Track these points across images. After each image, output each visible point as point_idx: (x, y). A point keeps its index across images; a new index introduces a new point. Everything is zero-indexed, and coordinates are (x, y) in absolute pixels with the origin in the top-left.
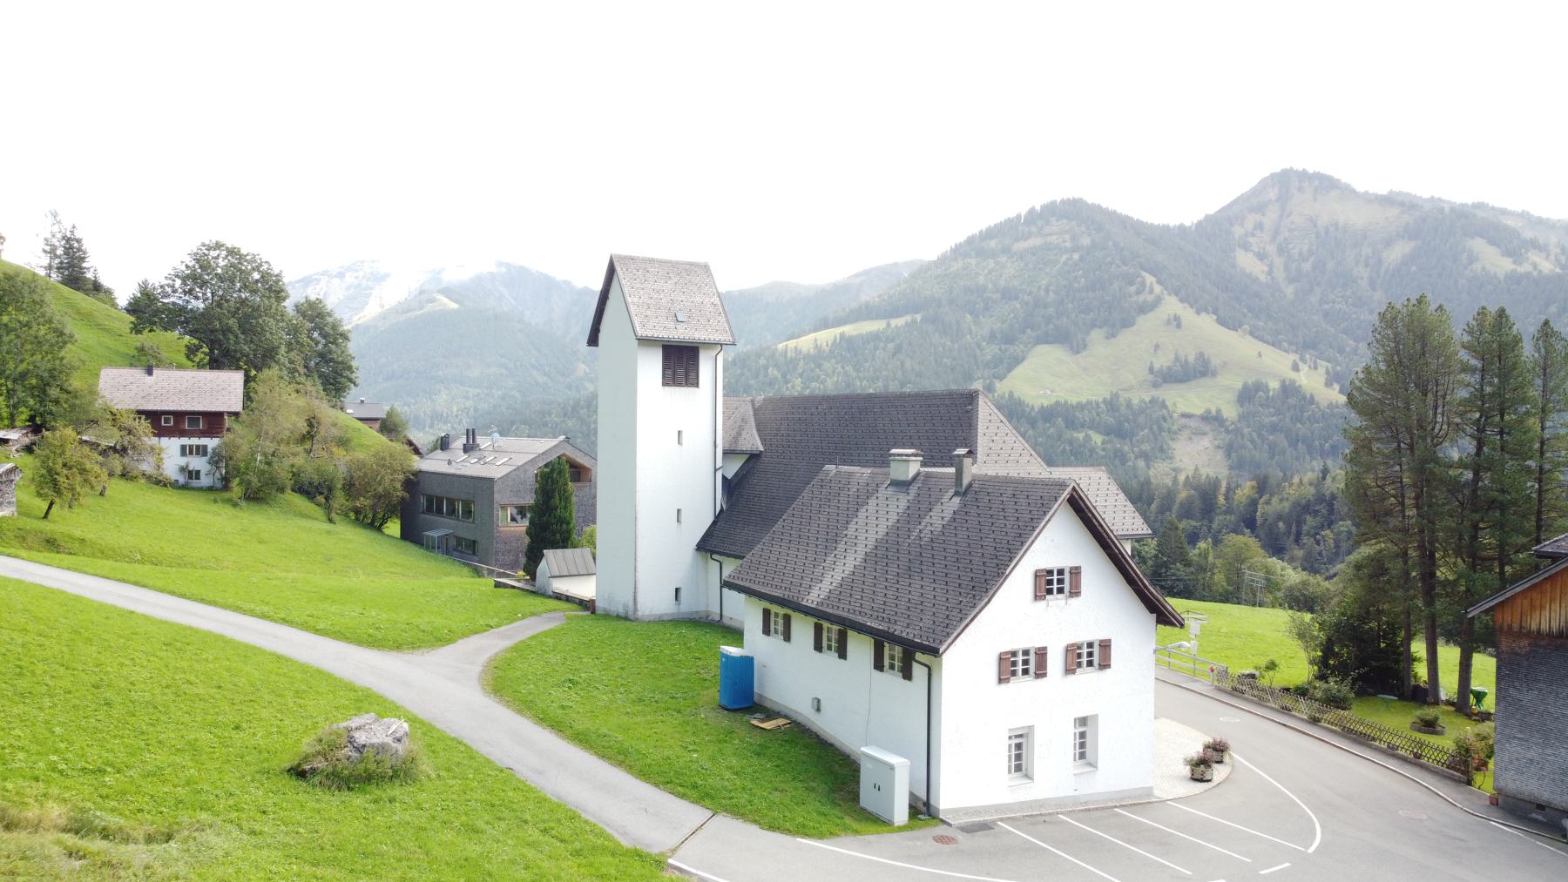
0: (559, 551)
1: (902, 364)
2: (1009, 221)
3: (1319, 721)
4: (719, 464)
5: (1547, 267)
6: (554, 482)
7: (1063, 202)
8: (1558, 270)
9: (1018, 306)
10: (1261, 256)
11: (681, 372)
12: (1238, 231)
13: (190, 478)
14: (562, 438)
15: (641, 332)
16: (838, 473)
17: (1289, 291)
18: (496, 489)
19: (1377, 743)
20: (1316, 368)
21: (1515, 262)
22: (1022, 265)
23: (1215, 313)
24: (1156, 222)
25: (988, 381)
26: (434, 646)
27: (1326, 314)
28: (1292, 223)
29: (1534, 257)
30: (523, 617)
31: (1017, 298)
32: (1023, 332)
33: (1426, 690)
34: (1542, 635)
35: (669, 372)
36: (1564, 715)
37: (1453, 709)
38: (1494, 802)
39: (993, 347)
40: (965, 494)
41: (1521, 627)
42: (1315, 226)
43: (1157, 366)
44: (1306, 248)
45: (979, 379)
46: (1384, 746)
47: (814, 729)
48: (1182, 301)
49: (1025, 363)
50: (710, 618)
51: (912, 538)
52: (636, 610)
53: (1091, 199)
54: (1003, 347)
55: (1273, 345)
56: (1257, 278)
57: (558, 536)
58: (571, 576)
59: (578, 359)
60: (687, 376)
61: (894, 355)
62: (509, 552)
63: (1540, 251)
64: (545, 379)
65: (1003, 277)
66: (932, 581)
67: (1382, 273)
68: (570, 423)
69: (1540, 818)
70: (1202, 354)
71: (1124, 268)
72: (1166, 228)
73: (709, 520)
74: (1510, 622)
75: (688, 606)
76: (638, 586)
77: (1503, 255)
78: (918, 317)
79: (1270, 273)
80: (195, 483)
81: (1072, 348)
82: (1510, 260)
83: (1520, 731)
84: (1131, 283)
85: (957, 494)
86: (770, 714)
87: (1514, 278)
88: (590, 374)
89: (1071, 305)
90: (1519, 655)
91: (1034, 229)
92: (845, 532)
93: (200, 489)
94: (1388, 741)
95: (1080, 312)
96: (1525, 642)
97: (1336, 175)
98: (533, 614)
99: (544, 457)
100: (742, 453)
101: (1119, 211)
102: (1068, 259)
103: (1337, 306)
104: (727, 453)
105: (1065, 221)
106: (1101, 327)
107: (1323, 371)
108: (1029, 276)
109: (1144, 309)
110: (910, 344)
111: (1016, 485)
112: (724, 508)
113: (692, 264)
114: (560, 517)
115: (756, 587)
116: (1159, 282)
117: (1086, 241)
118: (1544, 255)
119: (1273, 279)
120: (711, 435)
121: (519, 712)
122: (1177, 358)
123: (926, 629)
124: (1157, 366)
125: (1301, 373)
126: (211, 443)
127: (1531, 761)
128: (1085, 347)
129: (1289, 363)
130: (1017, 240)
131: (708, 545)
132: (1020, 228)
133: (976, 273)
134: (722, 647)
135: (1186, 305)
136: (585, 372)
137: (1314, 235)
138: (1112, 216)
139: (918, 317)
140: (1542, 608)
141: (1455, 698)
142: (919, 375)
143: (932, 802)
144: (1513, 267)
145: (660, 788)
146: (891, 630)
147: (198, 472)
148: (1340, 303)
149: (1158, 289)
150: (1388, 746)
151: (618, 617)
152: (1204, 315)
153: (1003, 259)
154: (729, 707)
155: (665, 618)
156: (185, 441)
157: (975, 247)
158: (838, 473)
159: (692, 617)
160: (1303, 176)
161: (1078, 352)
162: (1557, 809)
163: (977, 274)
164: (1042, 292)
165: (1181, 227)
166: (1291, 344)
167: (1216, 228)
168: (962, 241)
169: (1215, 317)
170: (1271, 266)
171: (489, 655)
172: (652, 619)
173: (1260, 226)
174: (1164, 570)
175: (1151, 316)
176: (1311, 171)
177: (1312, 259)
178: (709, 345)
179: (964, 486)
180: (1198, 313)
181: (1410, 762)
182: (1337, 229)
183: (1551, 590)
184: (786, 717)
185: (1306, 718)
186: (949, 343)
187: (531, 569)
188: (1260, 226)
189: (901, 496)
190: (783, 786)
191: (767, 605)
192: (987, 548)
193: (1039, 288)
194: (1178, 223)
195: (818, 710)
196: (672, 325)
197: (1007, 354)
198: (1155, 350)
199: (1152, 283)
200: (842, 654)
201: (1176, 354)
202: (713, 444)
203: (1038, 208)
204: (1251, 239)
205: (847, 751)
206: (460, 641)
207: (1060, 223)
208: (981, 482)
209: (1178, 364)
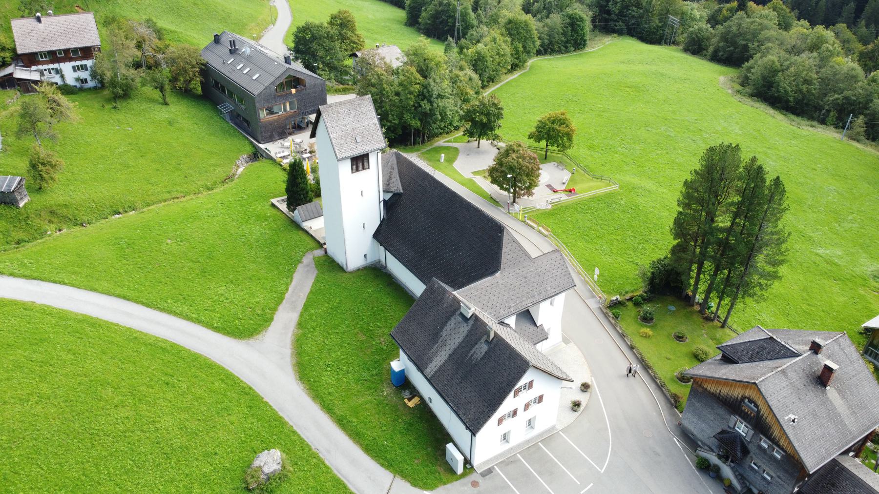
13: (83, 83)
33: (690, 297)
46: (653, 375)
62: (268, 131)
80: (86, 86)
93: (90, 89)
100: (392, 192)
120: (377, 186)
121: (313, 399)
126: (89, 63)
143: (472, 462)
147: (86, 80)
156: (74, 63)
174: (625, 11)
196: (354, 146)
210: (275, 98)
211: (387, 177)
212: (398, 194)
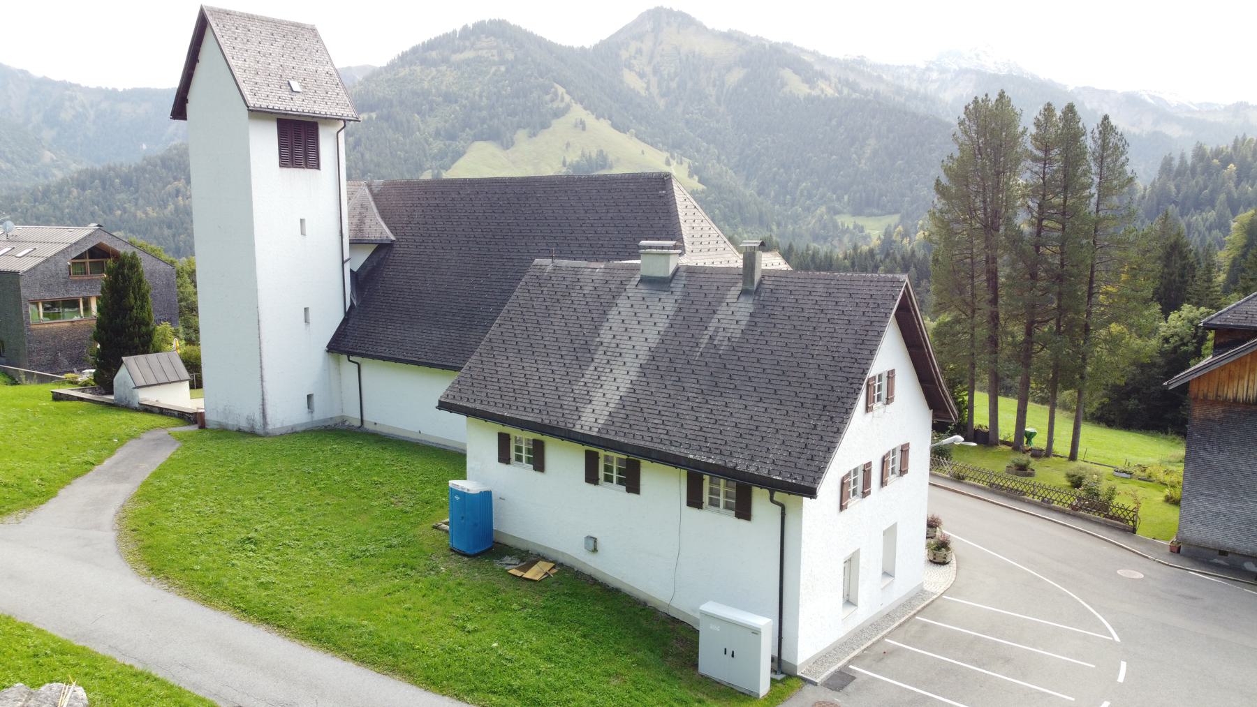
0: (141, 358)
1: (362, 155)
2: (446, 36)
3: (963, 478)
4: (346, 256)
5: (830, 92)
6: (127, 279)
7: (491, 22)
8: (836, 95)
9: (458, 108)
10: (641, 75)
11: (299, 150)
12: (624, 55)
14: (93, 226)
15: (252, 102)
16: (556, 268)
17: (662, 103)
18: (22, 284)
19: (1030, 497)
20: (681, 163)
21: (810, 88)
22: (459, 74)
23: (610, 119)
24: (563, 44)
25: (436, 171)
26: (29, 505)
27: (687, 122)
28: (663, 50)
29: (822, 84)
30: (122, 442)
31: (456, 102)
32: (463, 131)
34: (1239, 402)
35: (286, 151)
36: (1254, 473)
37: (1010, 448)
38: (1176, 550)
39: (438, 142)
40: (757, 292)
41: (1217, 396)
42: (679, 54)
43: (568, 160)
44: (673, 70)
45: (428, 169)
46: (984, 485)
47: (588, 571)
48: (585, 108)
49: (466, 157)
50: (347, 423)
51: (703, 346)
52: (265, 424)
53: (513, 21)
54: (447, 143)
55: (652, 145)
56: (638, 92)
57: (136, 340)
58: (159, 384)
59: (43, 147)
60: (306, 156)
61: (354, 148)
62: (45, 351)
63: (826, 80)
64: (9, 165)
65: (445, 83)
66: (758, 399)
67: (725, 91)
68: (41, 208)
69: (1222, 562)
70: (601, 152)
71: (541, 80)
72: (571, 49)
73: (339, 317)
74: (1205, 391)
75: (323, 412)
76: (265, 397)
77: (803, 82)
78: (374, 115)
79: (647, 89)
81: (502, 144)
82: (807, 86)
83: (1208, 489)
84: (547, 93)
85: (745, 292)
86: (528, 557)
87: (810, 99)
88: (57, 161)
89: (500, 109)
90: (1213, 421)
91: (468, 44)
92: (598, 339)
94: (1044, 495)
95: (508, 115)
96: (1218, 409)
97: (693, 15)
98: (131, 437)
99: (78, 246)
100: (370, 243)
101: (535, 33)
102: (496, 71)
103: (695, 117)
104: (354, 243)
105: (492, 38)
106: (524, 128)
107: (687, 166)
108: (466, 84)
109: (558, 114)
110: (368, 138)
111: (827, 282)
112: (355, 303)
113: (297, 26)
114: (137, 318)
115: (492, 410)
116: (568, 93)
117: (510, 56)
118: (828, 83)
119: (650, 93)
120: (335, 209)
121: (206, 601)
122: (583, 155)
123: (781, 463)
124: (568, 160)
125: (672, 167)
127: (1218, 514)
128: (513, 144)
129: (664, 160)
130: (454, 52)
131: (340, 345)
132: (457, 42)
133: (421, 79)
134: (451, 482)
135: (588, 112)
136: (52, 159)
137: (678, 61)
138: (529, 36)
139: (374, 115)
140: (1241, 378)
141: (1012, 439)
142: (378, 165)
144: (809, 91)
145: (465, 701)
146: (730, 465)
148: (696, 114)
149: (567, 98)
150: (1043, 500)
151: (241, 433)
152: (602, 119)
153: (444, 68)
154: (468, 552)
155: (298, 429)
157: (418, 56)
158: (556, 268)
159: (326, 424)
160: (670, 13)
161: (508, 148)
162: (1242, 555)
163: (422, 80)
164: (477, 98)
165: (582, 48)
166: (663, 145)
167: (608, 51)
168: (408, 50)
169: (610, 122)
170: (648, 83)
171: (113, 511)
172: (283, 431)
173: (639, 51)
175: (562, 120)
176: (675, 10)
177: (677, 79)
178: (330, 120)
179: (756, 283)
180: (598, 118)
181: (1069, 514)
182: (693, 56)
183: (1251, 363)
184: (544, 559)
185: (948, 476)
186: (401, 138)
187: (104, 383)
188: (639, 51)
189: (663, 295)
190: (612, 667)
191: (500, 428)
192: (819, 357)
193: (474, 93)
194: (580, 46)
195: (595, 550)
196: (286, 95)
197: (451, 148)
198: (567, 148)
199: (562, 94)
200: (539, 465)
201: (582, 151)
202: (338, 234)
203: (470, 26)
204: (633, 62)
205: (642, 597)
206: (62, 493)
207: (489, 39)
208: (773, 279)
209: (584, 159)
210: (65, 284)
211: (355, 220)
212: (387, 245)
